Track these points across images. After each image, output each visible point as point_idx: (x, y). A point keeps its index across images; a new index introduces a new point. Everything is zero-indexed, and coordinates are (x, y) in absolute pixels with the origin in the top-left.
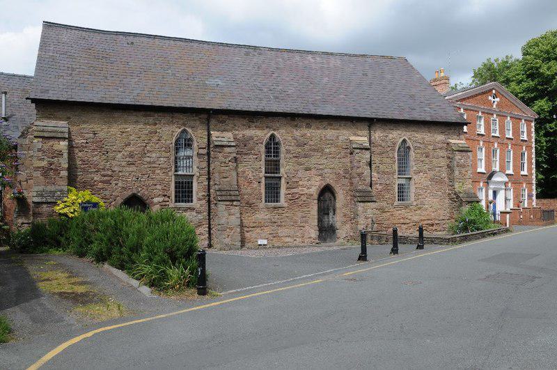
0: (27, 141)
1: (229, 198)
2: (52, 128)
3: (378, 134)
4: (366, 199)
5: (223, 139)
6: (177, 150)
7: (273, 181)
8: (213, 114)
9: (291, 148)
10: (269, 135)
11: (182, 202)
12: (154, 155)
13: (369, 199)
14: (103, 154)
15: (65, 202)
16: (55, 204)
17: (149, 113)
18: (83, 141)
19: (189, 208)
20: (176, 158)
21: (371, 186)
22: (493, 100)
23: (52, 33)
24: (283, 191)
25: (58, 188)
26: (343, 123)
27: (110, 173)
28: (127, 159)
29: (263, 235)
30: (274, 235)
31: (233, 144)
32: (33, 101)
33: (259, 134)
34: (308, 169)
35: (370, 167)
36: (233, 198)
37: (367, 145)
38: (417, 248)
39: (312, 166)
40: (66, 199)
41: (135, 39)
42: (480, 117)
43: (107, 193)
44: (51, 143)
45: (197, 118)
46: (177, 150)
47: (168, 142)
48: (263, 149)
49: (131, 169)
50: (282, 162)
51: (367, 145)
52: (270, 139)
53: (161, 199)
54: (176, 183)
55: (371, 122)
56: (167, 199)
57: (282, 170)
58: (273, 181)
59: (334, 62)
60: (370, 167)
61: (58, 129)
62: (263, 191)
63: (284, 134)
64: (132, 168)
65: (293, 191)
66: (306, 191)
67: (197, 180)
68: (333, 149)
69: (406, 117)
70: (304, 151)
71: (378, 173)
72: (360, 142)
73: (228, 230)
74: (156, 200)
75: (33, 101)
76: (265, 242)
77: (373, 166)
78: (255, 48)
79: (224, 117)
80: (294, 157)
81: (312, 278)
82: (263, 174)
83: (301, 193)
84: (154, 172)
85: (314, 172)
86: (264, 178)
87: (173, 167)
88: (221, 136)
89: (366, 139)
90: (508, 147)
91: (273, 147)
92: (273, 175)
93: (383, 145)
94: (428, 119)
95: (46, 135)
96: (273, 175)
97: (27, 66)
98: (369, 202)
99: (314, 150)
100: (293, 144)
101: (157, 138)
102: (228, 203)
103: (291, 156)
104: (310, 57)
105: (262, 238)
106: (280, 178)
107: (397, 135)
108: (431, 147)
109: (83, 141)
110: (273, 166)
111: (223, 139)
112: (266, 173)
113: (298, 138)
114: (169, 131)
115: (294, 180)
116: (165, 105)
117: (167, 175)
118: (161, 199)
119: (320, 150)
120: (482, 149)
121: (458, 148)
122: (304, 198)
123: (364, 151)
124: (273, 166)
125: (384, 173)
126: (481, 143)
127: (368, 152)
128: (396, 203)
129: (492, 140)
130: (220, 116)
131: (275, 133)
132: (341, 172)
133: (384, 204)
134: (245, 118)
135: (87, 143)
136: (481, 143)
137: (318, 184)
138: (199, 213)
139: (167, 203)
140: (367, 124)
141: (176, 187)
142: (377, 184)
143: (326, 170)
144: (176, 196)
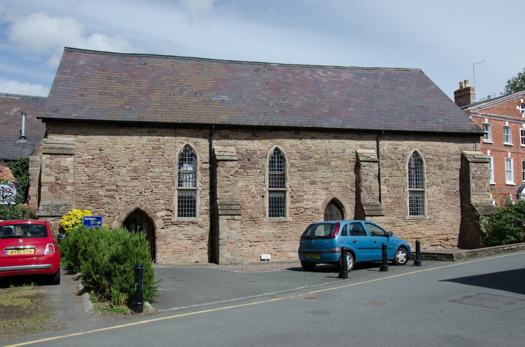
0: (38, 158)
1: (230, 212)
2: (61, 146)
3: (386, 145)
4: (374, 213)
5: (226, 154)
6: (181, 164)
7: (277, 195)
8: (215, 129)
9: (296, 162)
10: (273, 149)
11: (185, 216)
12: (157, 170)
13: (377, 213)
14: (109, 169)
15: (69, 215)
16: (60, 217)
17: (152, 129)
18: (90, 157)
19: (192, 222)
20: (179, 173)
21: (380, 200)
22: (521, 109)
23: (71, 57)
24: (288, 204)
25: (63, 202)
26: (350, 135)
27: (114, 187)
28: (132, 174)
29: (267, 250)
30: (278, 250)
31: (235, 158)
32: (44, 120)
33: (263, 147)
34: (313, 183)
35: (379, 180)
36: (234, 212)
37: (375, 158)
38: (414, 264)
39: (318, 180)
40: (70, 212)
41: (149, 59)
42: (507, 128)
43: (111, 207)
44: (58, 159)
45: (200, 133)
46: (181, 164)
47: (171, 157)
48: (267, 164)
49: (135, 184)
50: (288, 176)
51: (375, 158)
52: (275, 153)
53: (164, 213)
54: (179, 197)
55: (378, 135)
56: (170, 213)
57: (287, 184)
58: (277, 195)
59: (345, 75)
60: (379, 180)
61: (66, 146)
62: (267, 205)
63: (288, 145)
64: (136, 183)
65: (298, 205)
66: (311, 205)
67: (200, 194)
68: (340, 162)
69: (417, 129)
70: (312, 163)
71: (388, 186)
72: (368, 155)
73: (228, 244)
74: (159, 214)
75: (44, 120)
76: (268, 257)
77: (382, 179)
78: (266, 64)
79: (226, 132)
80: (298, 170)
81: (272, 297)
82: (266, 188)
83: (308, 207)
84: (156, 187)
85: (320, 185)
86: (267, 192)
87: (177, 181)
88: (223, 148)
89: (374, 151)
90: (507, 156)
91: (278, 159)
92: (277, 189)
93: (393, 157)
94: (440, 130)
95: (53, 151)
96: (277, 189)
97: (41, 91)
98: (377, 216)
99: (320, 163)
100: (298, 158)
101: (160, 154)
102: (229, 217)
103: (296, 170)
104: (320, 72)
105: (265, 253)
106: (284, 192)
107: (408, 147)
108: (444, 159)
109: (90, 157)
110: (278, 180)
111: (226, 154)
112: (270, 187)
113: (303, 151)
114: (175, 144)
115: (299, 194)
116: (169, 121)
117: (170, 189)
118: (164, 213)
119: (327, 164)
120: (510, 160)
121: (474, 160)
122: (309, 212)
123: (371, 163)
124: (278, 180)
125: (394, 186)
126: (509, 154)
127: (376, 164)
128: (408, 217)
129: (504, 149)
130: (223, 131)
131: (279, 147)
132: (349, 186)
133: (394, 218)
134: (248, 132)
135: (93, 159)
136: (509, 154)
137: (324, 197)
138: (201, 227)
139: (170, 217)
140: (375, 136)
141: (179, 202)
142: (386, 197)
143: (332, 184)
144: (179, 211)
